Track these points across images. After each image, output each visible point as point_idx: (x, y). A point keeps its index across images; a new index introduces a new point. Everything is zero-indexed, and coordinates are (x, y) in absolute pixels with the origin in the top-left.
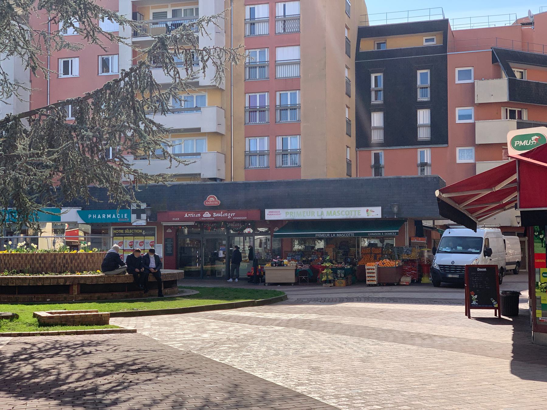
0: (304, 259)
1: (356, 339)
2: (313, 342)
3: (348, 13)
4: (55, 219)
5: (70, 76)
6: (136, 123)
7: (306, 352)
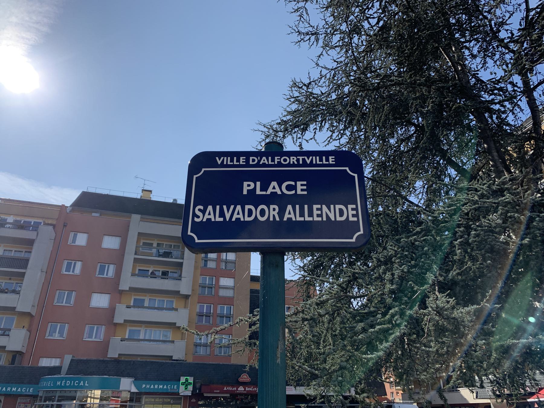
5: (71, 273)
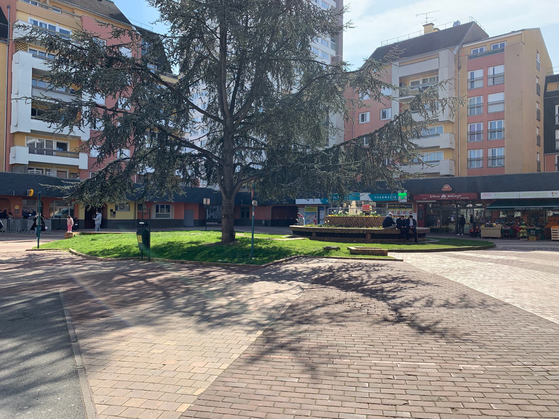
0: (507, 223)
1: (545, 274)
2: (515, 274)
3: (538, 69)
4: (357, 198)
6: (402, 144)
7: (509, 279)
